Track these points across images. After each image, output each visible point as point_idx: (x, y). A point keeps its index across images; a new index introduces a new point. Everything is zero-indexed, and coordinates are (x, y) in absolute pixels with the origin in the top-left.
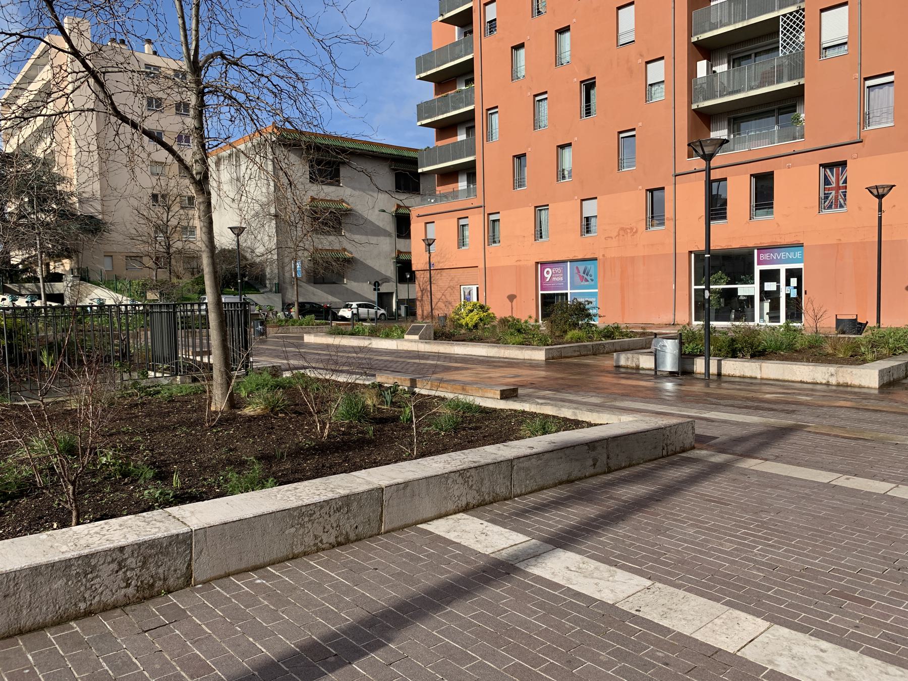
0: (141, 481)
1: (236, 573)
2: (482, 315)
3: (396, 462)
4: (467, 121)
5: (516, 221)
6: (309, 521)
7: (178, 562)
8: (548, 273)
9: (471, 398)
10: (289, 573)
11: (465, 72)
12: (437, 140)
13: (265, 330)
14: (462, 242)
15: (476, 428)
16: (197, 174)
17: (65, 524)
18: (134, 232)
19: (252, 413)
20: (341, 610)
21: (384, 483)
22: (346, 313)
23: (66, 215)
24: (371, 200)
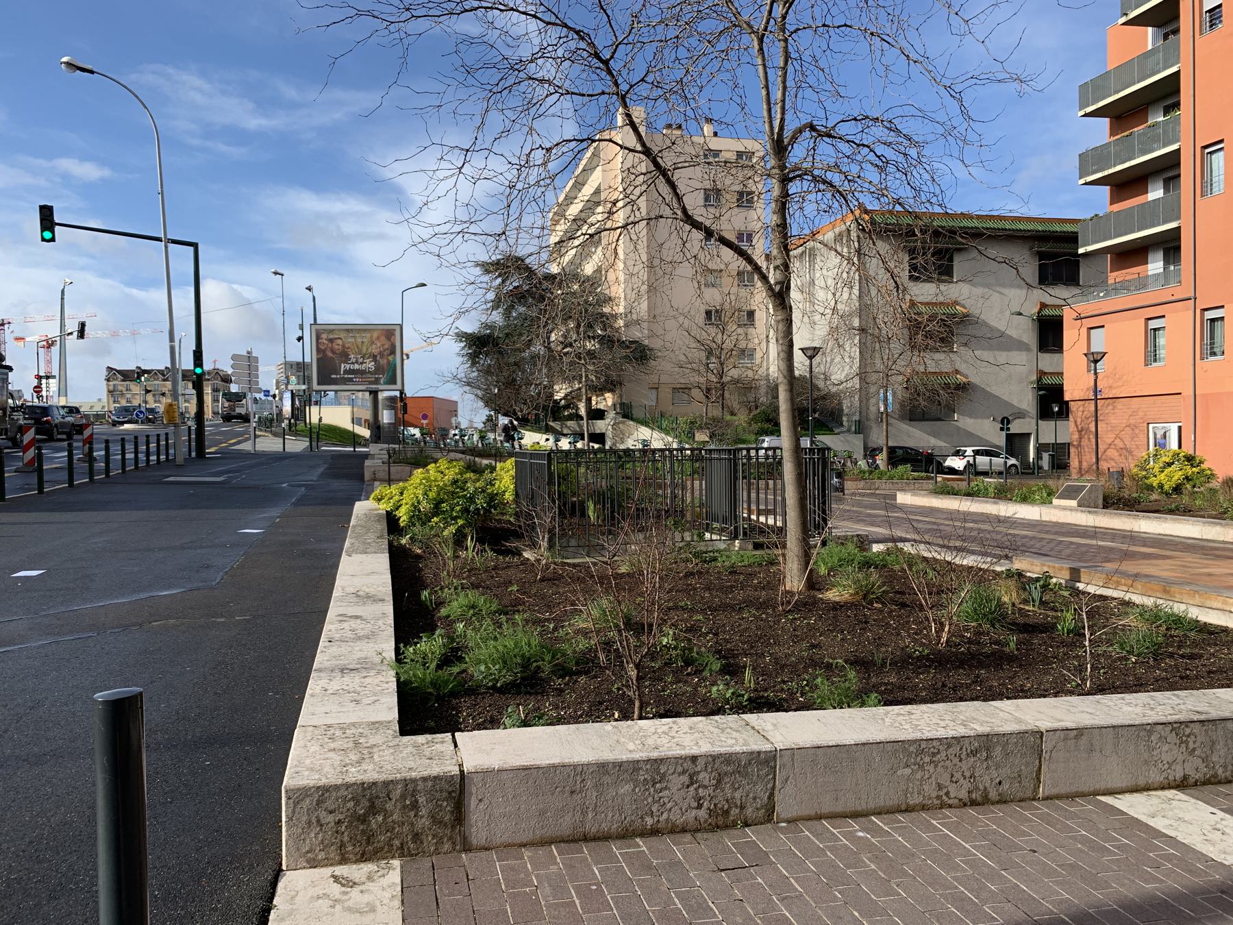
0: (706, 673)
1: (832, 816)
2: (1190, 471)
3: (1056, 695)
4: (1167, 169)
6: (931, 762)
7: (759, 787)
9: (1183, 607)
10: (901, 830)
11: (1166, 94)
12: (1111, 204)
13: (842, 484)
14: (1152, 355)
15: (1192, 657)
16: (776, 283)
17: (626, 716)
18: (683, 358)
19: (837, 599)
20: (984, 902)
21: (1044, 725)
22: (957, 463)
23: (609, 342)
24: (1000, 299)
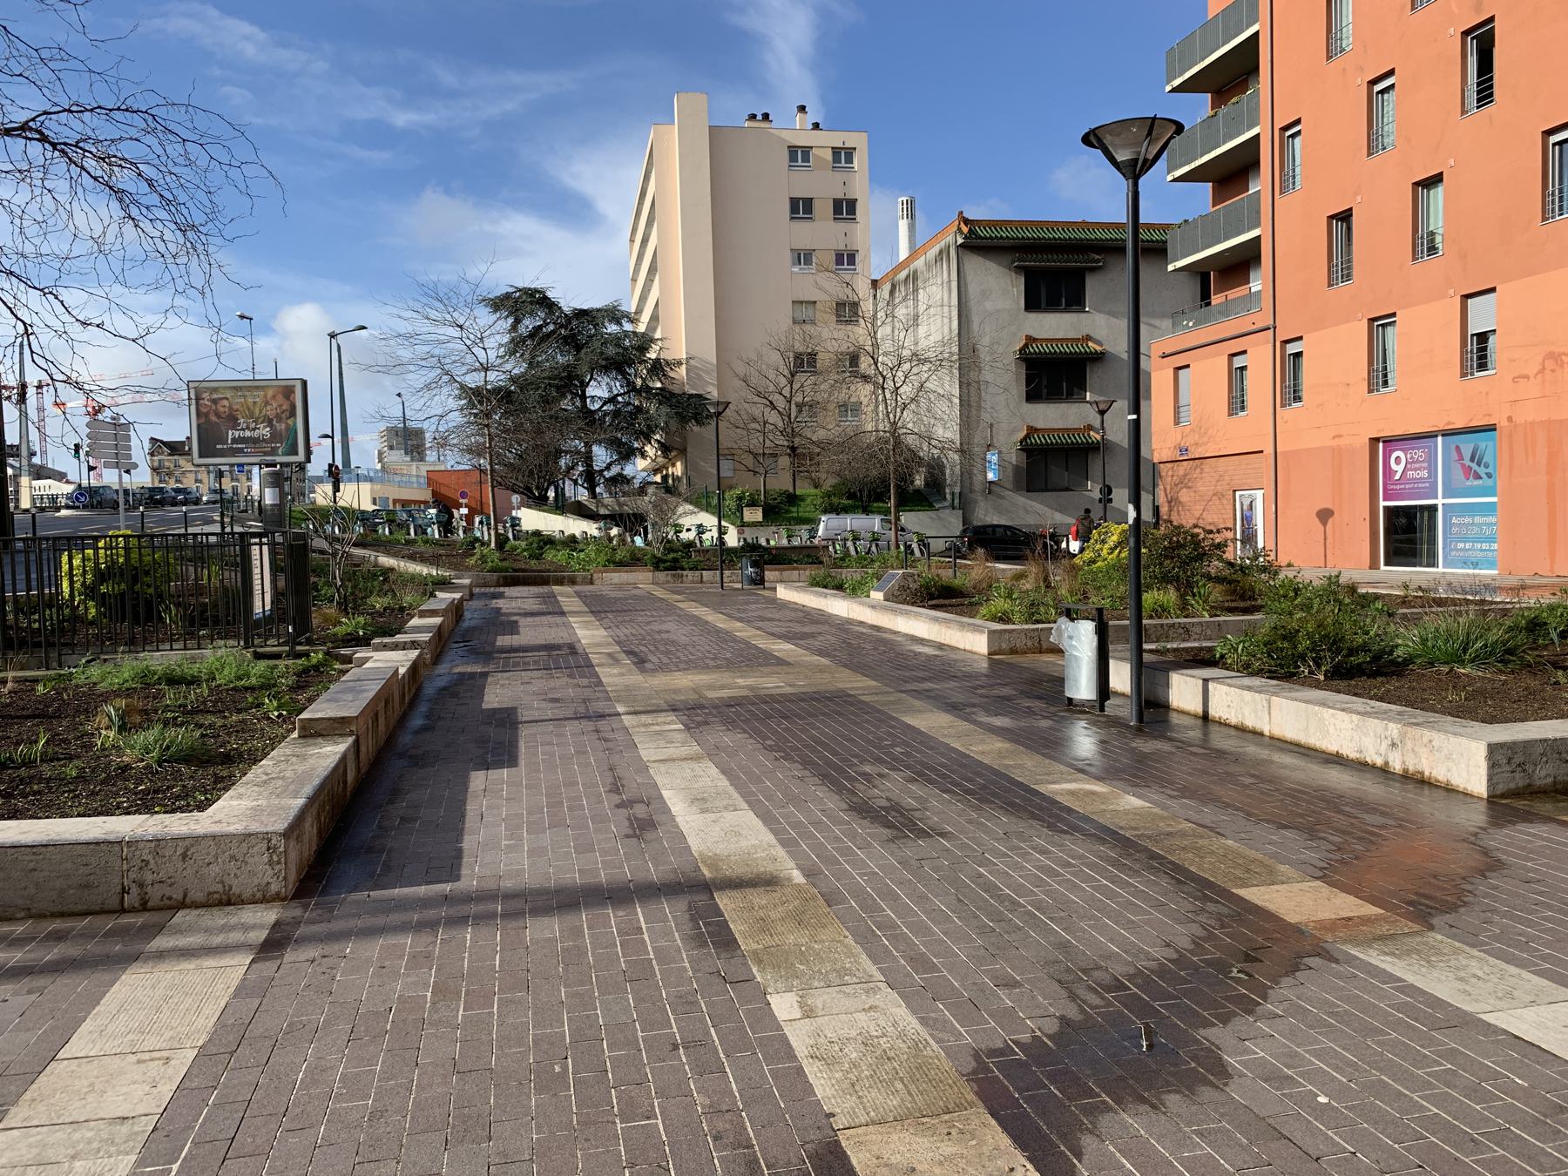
5: (1335, 354)
8: (1398, 460)
14: (1237, 403)
